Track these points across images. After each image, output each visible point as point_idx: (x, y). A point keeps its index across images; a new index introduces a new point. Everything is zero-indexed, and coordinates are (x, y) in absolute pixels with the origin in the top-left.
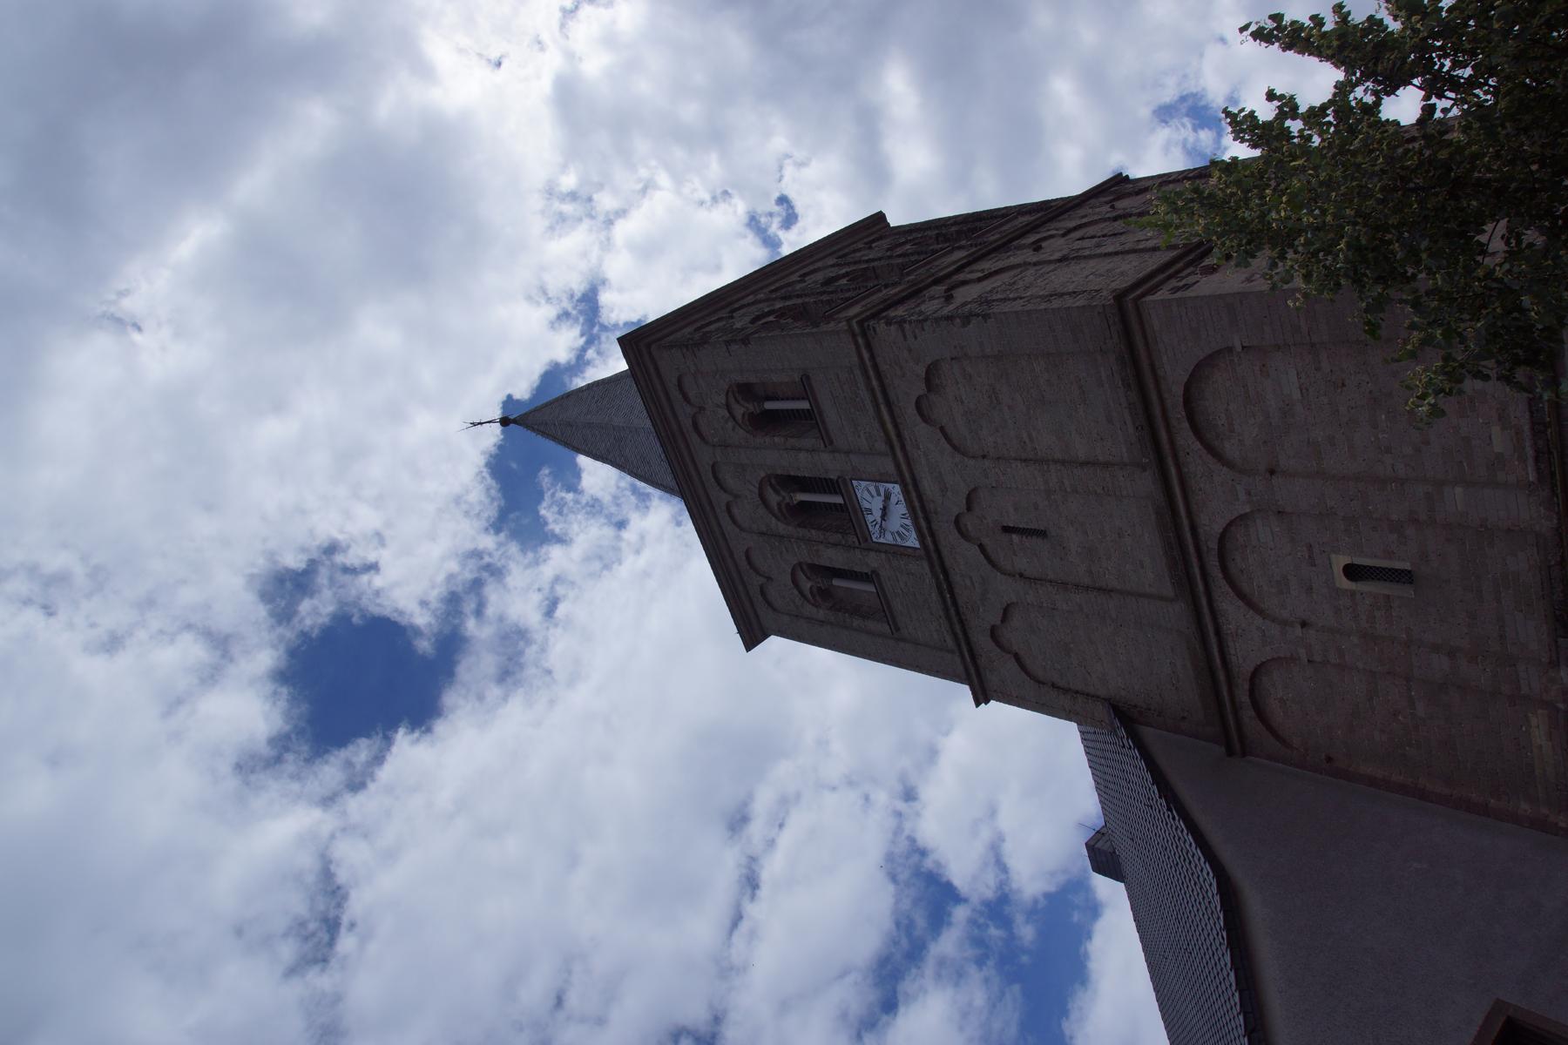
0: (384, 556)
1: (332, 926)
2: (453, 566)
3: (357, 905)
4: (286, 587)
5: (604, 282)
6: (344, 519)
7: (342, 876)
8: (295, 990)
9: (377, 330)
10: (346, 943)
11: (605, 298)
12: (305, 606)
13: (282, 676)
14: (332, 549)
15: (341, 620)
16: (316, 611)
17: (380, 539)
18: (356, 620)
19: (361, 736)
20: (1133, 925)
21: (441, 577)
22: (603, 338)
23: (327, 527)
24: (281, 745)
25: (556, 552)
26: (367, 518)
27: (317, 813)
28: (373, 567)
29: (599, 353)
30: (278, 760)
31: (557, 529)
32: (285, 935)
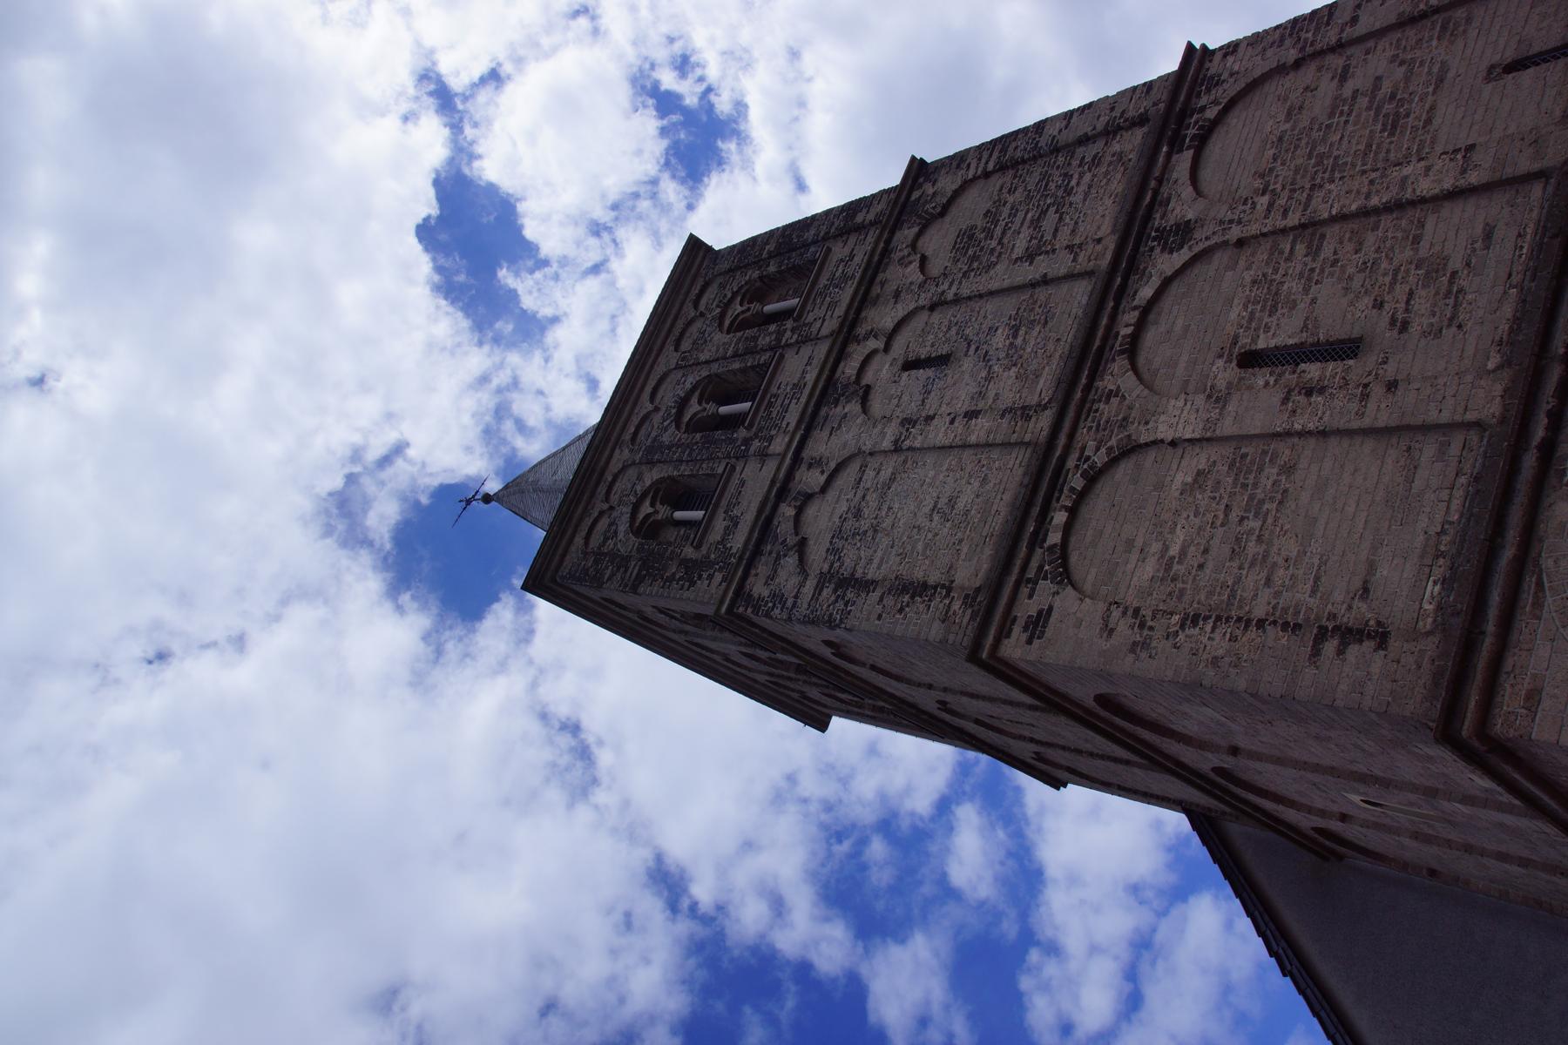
0: (407, 430)
1: (584, 753)
2: (469, 403)
3: (594, 725)
4: (342, 512)
5: (432, 51)
6: (343, 427)
7: (563, 711)
8: (584, 814)
9: (257, 236)
10: (604, 758)
11: (445, 66)
12: (372, 520)
13: (394, 591)
14: (356, 455)
15: (409, 500)
16: (383, 515)
17: (390, 417)
18: (425, 500)
19: (490, 603)
20: (1307, 10)
21: (466, 419)
22: (472, 109)
23: (338, 436)
24: (434, 642)
25: (558, 334)
26: (368, 408)
27: (502, 681)
28: (399, 449)
29: (476, 125)
30: (439, 652)
31: (547, 311)
32: (548, 780)
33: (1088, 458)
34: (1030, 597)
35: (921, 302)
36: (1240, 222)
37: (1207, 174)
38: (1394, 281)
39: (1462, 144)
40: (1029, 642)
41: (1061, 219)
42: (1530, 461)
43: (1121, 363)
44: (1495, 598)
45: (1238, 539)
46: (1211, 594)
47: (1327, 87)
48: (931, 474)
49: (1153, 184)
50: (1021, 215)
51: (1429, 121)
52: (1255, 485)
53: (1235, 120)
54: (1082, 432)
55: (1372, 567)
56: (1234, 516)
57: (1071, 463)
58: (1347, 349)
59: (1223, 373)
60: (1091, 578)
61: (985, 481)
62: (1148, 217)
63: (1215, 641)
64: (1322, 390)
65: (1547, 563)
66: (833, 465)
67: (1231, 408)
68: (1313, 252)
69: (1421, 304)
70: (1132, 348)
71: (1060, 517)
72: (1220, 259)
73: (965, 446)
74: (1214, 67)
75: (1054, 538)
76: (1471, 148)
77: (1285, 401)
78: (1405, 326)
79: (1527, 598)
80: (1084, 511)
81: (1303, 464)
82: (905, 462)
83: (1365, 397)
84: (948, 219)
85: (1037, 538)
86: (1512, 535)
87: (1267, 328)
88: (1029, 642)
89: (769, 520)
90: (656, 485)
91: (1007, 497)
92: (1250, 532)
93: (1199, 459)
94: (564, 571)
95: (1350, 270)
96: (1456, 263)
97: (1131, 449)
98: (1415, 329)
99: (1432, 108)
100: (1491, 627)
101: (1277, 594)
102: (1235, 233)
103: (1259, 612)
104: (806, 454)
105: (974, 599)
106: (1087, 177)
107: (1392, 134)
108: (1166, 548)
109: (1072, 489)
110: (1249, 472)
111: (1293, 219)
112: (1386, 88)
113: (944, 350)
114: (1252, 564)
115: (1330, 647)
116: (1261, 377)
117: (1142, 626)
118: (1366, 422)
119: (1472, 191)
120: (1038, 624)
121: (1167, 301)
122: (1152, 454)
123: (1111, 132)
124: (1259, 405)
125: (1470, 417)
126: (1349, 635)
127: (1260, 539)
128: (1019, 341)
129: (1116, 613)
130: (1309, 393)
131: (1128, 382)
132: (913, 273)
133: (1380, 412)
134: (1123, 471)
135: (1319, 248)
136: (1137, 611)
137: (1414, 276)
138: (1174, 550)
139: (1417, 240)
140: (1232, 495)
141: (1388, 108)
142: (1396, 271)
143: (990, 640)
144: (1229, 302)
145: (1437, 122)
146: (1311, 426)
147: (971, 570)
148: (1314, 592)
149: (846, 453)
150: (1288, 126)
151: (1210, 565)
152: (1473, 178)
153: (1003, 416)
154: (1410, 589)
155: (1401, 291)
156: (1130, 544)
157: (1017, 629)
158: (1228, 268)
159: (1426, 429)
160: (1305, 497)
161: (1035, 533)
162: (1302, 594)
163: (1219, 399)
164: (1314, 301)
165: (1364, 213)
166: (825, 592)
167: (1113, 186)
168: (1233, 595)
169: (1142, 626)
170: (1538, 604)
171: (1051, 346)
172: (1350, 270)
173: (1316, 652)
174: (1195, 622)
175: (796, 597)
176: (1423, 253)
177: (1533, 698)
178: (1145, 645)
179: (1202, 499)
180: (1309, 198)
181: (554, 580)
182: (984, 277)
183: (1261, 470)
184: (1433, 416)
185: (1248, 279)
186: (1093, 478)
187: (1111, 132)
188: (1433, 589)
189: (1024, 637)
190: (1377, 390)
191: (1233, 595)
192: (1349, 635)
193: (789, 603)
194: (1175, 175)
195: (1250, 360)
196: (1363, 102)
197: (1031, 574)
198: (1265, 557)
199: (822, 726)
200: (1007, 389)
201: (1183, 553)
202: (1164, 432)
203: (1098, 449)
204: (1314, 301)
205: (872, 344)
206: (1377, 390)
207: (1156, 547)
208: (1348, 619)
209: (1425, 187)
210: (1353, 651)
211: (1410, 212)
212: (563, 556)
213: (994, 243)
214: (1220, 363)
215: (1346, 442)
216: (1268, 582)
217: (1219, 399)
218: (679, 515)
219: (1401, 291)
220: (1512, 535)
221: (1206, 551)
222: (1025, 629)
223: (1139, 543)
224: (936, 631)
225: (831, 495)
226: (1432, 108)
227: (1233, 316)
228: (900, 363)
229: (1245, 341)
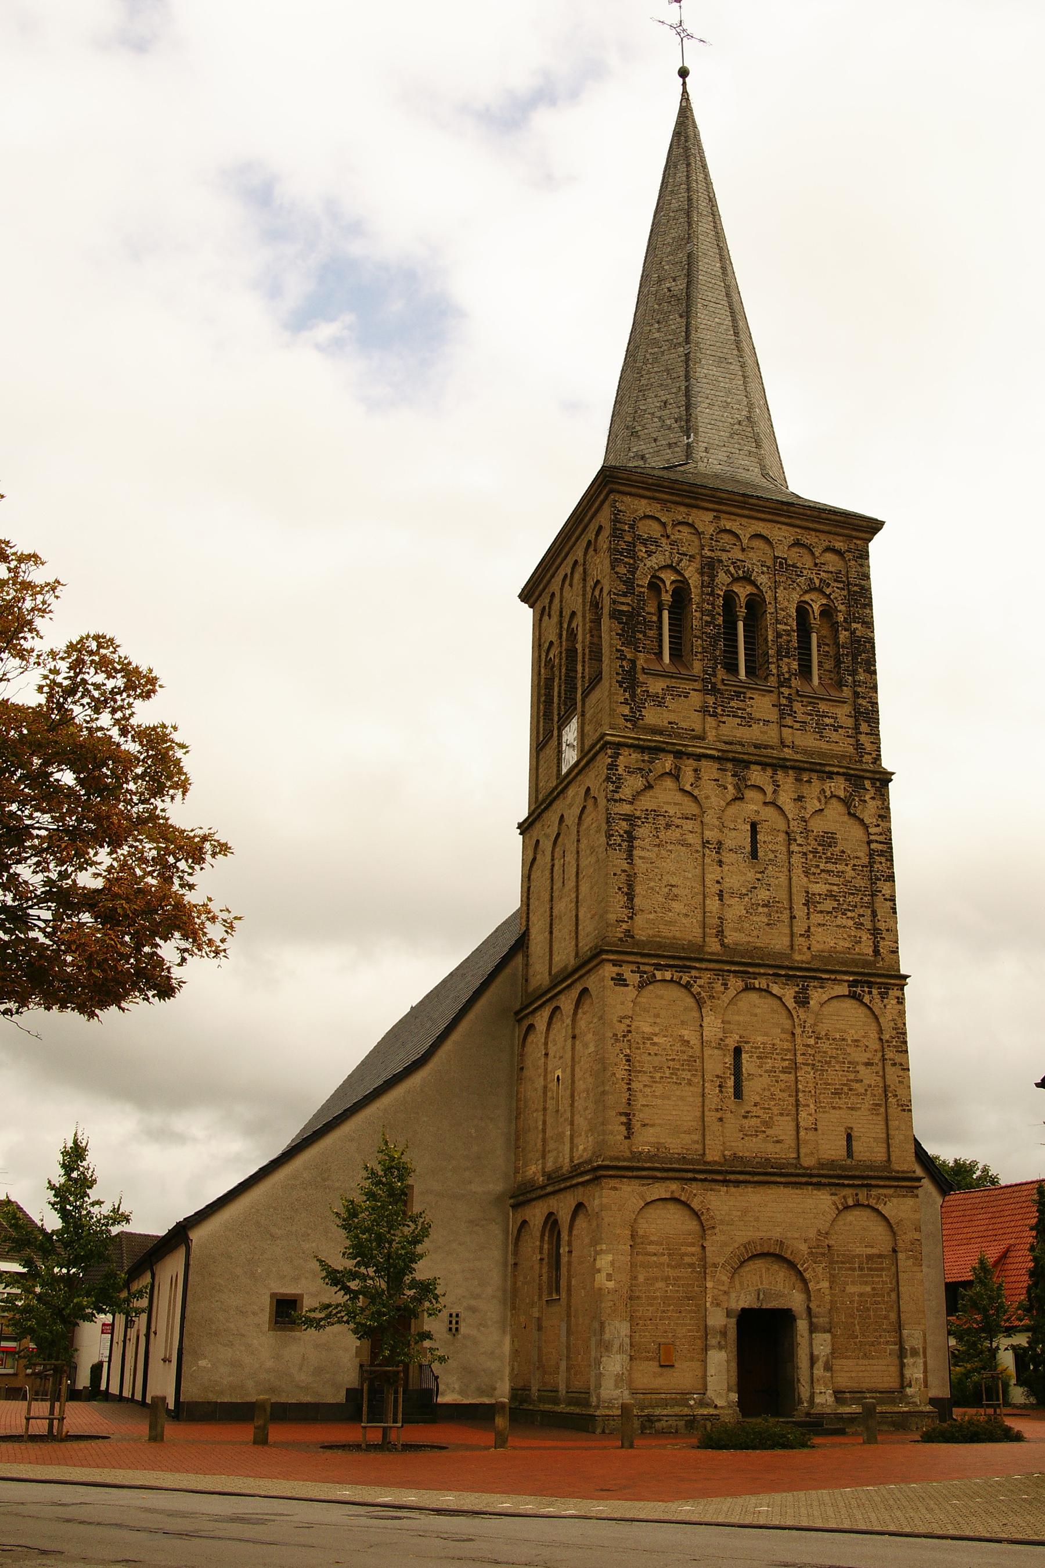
33: (695, 982)
34: (632, 971)
35: (792, 823)
36: (803, 1032)
37: (835, 1003)
38: (765, 1109)
39: (818, 1127)
40: (612, 979)
41: (828, 912)
42: (690, 1175)
43: (740, 984)
44: (644, 1173)
45: (661, 1068)
46: (639, 1062)
47: (864, 1057)
48: (690, 876)
49: (833, 977)
50: (836, 880)
51: (834, 1108)
52: (683, 1070)
53: (862, 1011)
54: (708, 975)
55: (652, 1126)
56: (671, 1063)
57: (694, 973)
58: (738, 1093)
59: (732, 1042)
60: (644, 1000)
61: (686, 915)
62: (815, 978)
63: (621, 1073)
64: (721, 1091)
65: (657, 1185)
66: (696, 793)
67: (716, 1051)
68: (784, 1071)
69: (754, 1122)
70: (748, 988)
71: (668, 975)
72: (787, 1023)
73: (704, 897)
74: (894, 993)
75: (659, 975)
76: (816, 1129)
77: (718, 1076)
78: (745, 1117)
79: (645, 1182)
80: (672, 986)
81: (691, 1089)
82: (697, 851)
83: (717, 1110)
84: (846, 818)
85: (658, 967)
86: (665, 1175)
87: (750, 1057)
88: (612, 979)
89: (663, 750)
90: (685, 582)
91: (678, 935)
92: (664, 1073)
93: (694, 1041)
94: (617, 497)
95: (772, 1089)
96: (769, 1132)
97: (700, 1003)
98: (745, 1121)
99: (840, 1108)
100: (635, 1173)
101: (641, 1091)
102: (798, 1031)
103: (634, 1085)
104: (704, 763)
105: (628, 936)
106: (850, 923)
107: (832, 1093)
108: (656, 1035)
109: (681, 978)
110: (688, 1065)
111: (800, 1059)
112: (855, 1086)
113: (760, 854)
114: (652, 1077)
115: (624, 1119)
116: (729, 1060)
117: (624, 1036)
118: (707, 1113)
119: (798, 1133)
120: (620, 981)
121: (770, 1000)
122: (697, 1015)
123: (875, 932)
124: (717, 1063)
125: (707, 1152)
126: (628, 1125)
127: (662, 1078)
128: (761, 910)
129: (628, 1021)
130: (720, 1086)
131: (732, 992)
132: (813, 805)
133: (711, 1117)
134: (690, 1001)
135: (785, 1072)
136: (629, 1031)
137: (766, 1117)
138: (656, 1039)
139: (781, 1114)
140: (679, 1060)
141: (846, 1089)
142: (769, 1109)
143: (612, 957)
144: (766, 1034)
145: (833, 1111)
146: (706, 1090)
147: (643, 928)
148: (643, 1105)
149: (703, 801)
150: (849, 1042)
151: (649, 1058)
152: (802, 1133)
153: (719, 918)
154: (645, 1141)
155: (760, 1113)
156: (657, 1016)
157: (616, 969)
158: (783, 1029)
159: (704, 1135)
160: (678, 1093)
161: (660, 965)
162: (642, 1101)
163: (720, 1045)
164: (761, 1076)
165: (797, 1091)
166: (624, 824)
167: (841, 943)
168: (640, 1072)
169: (624, 1036)
170: (643, 1185)
171: (755, 933)
172: (772, 1089)
173: (621, 1114)
174: (628, 1061)
175: (621, 800)
176: (775, 1118)
177: (615, 1189)
178: (617, 1040)
179: (678, 1047)
180: (808, 1065)
181: (611, 491)
182: (800, 871)
183: (689, 1071)
184: (707, 1138)
185: (775, 1041)
186: (687, 987)
187: (875, 932)
188: (646, 1148)
189: (614, 975)
190: (719, 1115)
191: (640, 1072)
192: (628, 1125)
193: (617, 796)
194: (836, 987)
195: (738, 1052)
196: (852, 1076)
197: (642, 968)
198: (655, 1082)
199: (528, 595)
200: (736, 909)
201: (655, 1044)
202: (707, 1020)
203: (700, 986)
204: (761, 1076)
205: (769, 789)
206: (719, 1115)
207: (657, 1030)
208: (634, 1122)
209: (803, 1114)
210: (623, 1128)
211: (794, 1109)
212: (631, 494)
213: (822, 866)
214: (737, 1038)
215: (700, 1104)
216: (645, 1086)
217: (720, 1045)
218: (666, 614)
219: (760, 1113)
220: (665, 1175)
221: (656, 1054)
222: (618, 974)
223: (658, 1020)
224: (612, 917)
225: (679, 797)
226: (840, 1108)
227: (759, 1038)
228: (757, 819)
229: (747, 1047)
